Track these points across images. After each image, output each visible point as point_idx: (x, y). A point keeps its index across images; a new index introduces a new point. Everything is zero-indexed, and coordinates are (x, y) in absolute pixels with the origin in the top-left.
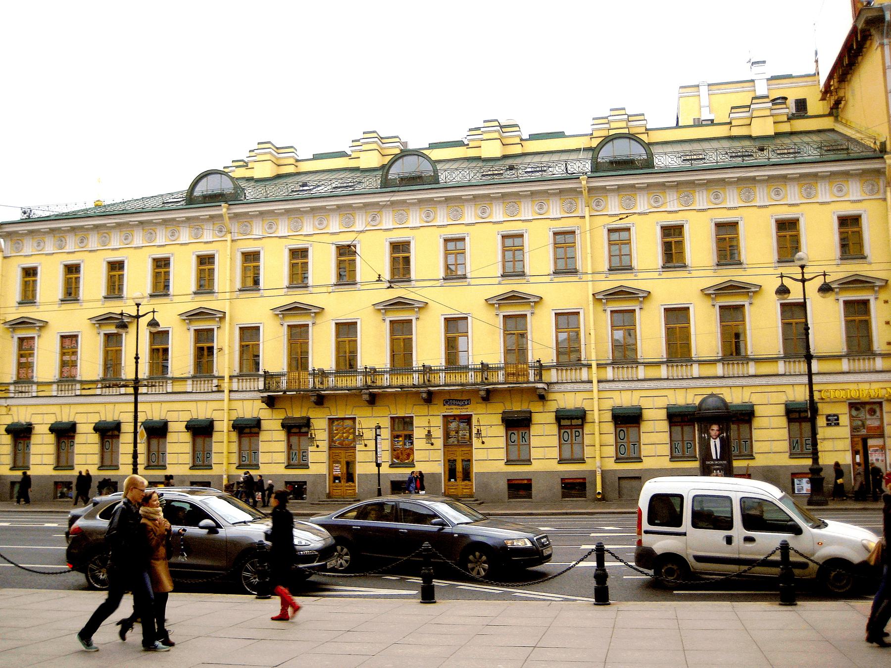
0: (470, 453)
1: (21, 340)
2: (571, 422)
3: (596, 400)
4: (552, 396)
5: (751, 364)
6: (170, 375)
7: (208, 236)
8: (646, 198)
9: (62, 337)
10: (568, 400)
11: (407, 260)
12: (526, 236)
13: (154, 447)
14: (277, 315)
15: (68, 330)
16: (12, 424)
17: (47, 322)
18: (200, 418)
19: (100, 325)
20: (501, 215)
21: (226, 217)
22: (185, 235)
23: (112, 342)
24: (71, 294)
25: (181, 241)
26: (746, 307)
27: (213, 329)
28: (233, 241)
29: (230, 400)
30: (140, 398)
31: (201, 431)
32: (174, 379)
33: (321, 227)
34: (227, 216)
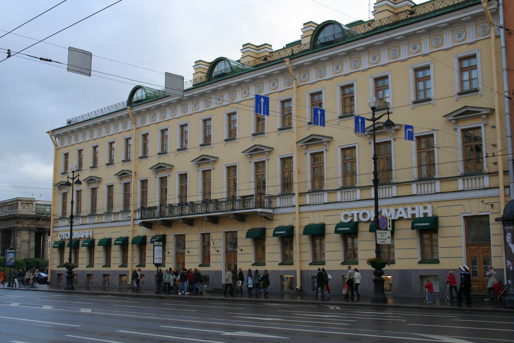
0: (489, 251)
1: (204, 172)
2: (286, 237)
3: (297, 218)
4: (275, 218)
5: (394, 188)
6: (97, 213)
7: (179, 113)
8: (474, 27)
9: (343, 149)
10: (284, 221)
11: (352, 98)
12: (478, 56)
13: (427, 242)
14: (450, 120)
15: (231, 163)
16: (310, 225)
17: (273, 148)
18: (316, 223)
19: (307, 146)
20: (387, 59)
21: (290, 69)
22: (330, 71)
23: (259, 166)
24: (232, 136)
25: (445, 46)
26: (325, 152)
27: (265, 161)
28: (298, 87)
29: (300, 213)
30: (74, 228)
31: (316, 233)
32: (397, 184)
33: (461, 39)
34: (489, 12)
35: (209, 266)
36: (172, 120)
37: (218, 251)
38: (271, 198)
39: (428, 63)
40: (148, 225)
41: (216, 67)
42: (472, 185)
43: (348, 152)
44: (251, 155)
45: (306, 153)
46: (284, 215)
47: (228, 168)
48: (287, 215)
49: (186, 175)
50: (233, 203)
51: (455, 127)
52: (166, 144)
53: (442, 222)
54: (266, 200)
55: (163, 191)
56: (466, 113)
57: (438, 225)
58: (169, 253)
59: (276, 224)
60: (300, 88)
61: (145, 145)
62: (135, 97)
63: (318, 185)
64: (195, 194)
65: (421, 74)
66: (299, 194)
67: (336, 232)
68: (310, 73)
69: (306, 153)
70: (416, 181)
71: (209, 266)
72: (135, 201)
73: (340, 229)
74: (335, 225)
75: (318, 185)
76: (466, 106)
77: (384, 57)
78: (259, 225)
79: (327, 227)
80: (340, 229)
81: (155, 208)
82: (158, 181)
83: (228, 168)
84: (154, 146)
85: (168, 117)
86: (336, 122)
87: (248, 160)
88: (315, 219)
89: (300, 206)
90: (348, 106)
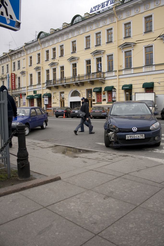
9: (145, 47)
16: (107, 87)
25: (141, 12)
35: (102, 103)
36: (56, 44)
37: (58, 100)
38: (104, 73)
39: (100, 31)
40: (50, 88)
41: (75, 20)
42: (146, 70)
43: (110, 57)
44: (122, 48)
45: (122, 52)
46: (109, 80)
47: (30, 75)
48: (146, 76)
49: (20, 77)
50: (89, 76)
51: (51, 68)
52: (49, 57)
53: (134, 86)
54: (102, 74)
55: (55, 75)
56: (127, 45)
57: (154, 86)
58: (65, 99)
59: (105, 85)
60: (119, 22)
61: (31, 61)
62: (75, 20)
63: (128, 65)
64: (68, 74)
65: (148, 19)
66: (43, 84)
67: (122, 89)
68: (100, 24)
69: (122, 52)
70: (144, 66)
71: (102, 103)
72: (44, 79)
73: (124, 88)
74: (122, 86)
75: (128, 65)
76: (97, 50)
77: (88, 29)
78: (98, 86)
79: (102, 88)
80: (124, 88)
81: (51, 80)
82: (71, 66)
83: (30, 75)
84: (93, 42)
85: (19, 56)
86: (59, 58)
87: (70, 63)
88: (127, 82)
89: (43, 87)
90: (110, 38)
